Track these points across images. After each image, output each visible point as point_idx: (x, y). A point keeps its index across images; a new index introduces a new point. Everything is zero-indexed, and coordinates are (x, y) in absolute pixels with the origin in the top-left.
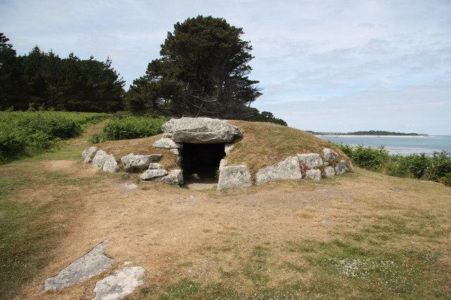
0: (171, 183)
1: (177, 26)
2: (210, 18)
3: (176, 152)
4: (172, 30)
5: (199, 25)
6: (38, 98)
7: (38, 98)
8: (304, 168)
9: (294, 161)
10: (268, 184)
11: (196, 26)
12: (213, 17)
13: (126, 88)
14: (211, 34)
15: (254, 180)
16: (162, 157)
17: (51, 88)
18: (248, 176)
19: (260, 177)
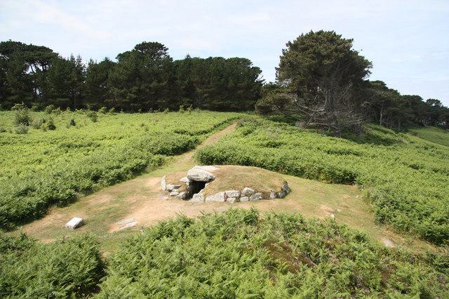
0: (179, 198)
1: (289, 44)
2: (320, 33)
3: (188, 184)
4: (255, 65)
5: (308, 42)
6: (188, 100)
7: (188, 100)
8: (226, 197)
9: (222, 194)
10: (210, 202)
11: (304, 44)
12: (324, 31)
13: (365, 79)
14: (314, 53)
15: (205, 200)
16: (145, 166)
17: (199, 90)
18: (203, 198)
19: (207, 199)
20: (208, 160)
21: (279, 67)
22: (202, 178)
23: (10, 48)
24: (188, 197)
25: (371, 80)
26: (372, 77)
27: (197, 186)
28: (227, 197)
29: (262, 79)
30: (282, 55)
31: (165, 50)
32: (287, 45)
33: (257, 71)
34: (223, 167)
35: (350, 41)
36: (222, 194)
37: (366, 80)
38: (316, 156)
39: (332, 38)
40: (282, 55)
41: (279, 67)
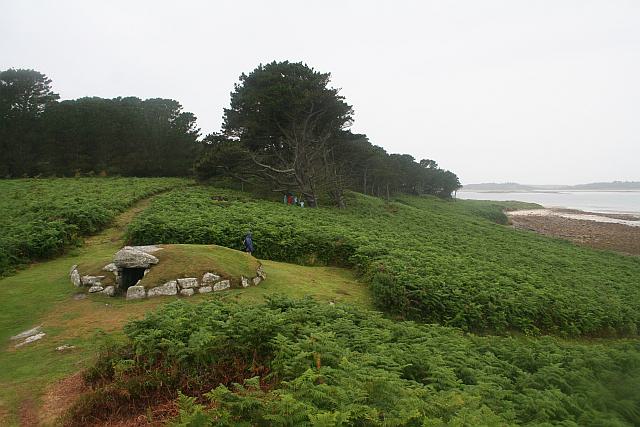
4: (185, 110)
9: (173, 284)
20: (138, 238)
21: (230, 108)
22: (139, 262)
23: (9, 75)
24: (120, 292)
25: (354, 132)
26: (355, 128)
27: (131, 274)
28: (181, 288)
29: (196, 129)
30: (234, 91)
31: (46, 83)
32: (241, 79)
33: (190, 117)
34: (172, 247)
35: (326, 76)
36: (173, 284)
37: (345, 130)
38: (324, 395)
39: (298, 71)
40: (234, 91)
41: (230, 108)
